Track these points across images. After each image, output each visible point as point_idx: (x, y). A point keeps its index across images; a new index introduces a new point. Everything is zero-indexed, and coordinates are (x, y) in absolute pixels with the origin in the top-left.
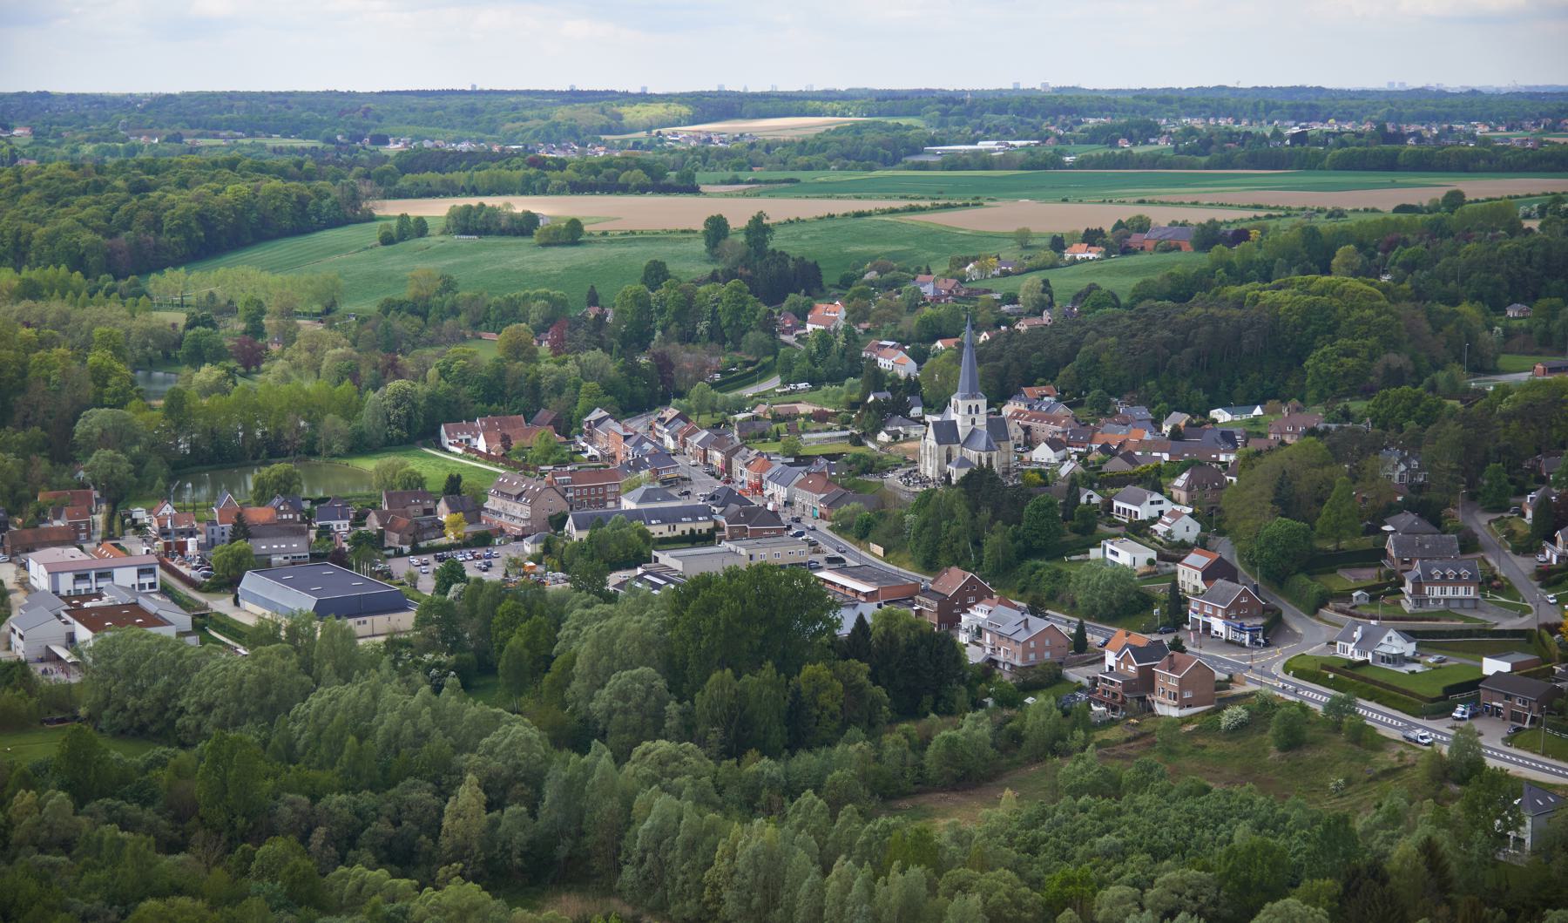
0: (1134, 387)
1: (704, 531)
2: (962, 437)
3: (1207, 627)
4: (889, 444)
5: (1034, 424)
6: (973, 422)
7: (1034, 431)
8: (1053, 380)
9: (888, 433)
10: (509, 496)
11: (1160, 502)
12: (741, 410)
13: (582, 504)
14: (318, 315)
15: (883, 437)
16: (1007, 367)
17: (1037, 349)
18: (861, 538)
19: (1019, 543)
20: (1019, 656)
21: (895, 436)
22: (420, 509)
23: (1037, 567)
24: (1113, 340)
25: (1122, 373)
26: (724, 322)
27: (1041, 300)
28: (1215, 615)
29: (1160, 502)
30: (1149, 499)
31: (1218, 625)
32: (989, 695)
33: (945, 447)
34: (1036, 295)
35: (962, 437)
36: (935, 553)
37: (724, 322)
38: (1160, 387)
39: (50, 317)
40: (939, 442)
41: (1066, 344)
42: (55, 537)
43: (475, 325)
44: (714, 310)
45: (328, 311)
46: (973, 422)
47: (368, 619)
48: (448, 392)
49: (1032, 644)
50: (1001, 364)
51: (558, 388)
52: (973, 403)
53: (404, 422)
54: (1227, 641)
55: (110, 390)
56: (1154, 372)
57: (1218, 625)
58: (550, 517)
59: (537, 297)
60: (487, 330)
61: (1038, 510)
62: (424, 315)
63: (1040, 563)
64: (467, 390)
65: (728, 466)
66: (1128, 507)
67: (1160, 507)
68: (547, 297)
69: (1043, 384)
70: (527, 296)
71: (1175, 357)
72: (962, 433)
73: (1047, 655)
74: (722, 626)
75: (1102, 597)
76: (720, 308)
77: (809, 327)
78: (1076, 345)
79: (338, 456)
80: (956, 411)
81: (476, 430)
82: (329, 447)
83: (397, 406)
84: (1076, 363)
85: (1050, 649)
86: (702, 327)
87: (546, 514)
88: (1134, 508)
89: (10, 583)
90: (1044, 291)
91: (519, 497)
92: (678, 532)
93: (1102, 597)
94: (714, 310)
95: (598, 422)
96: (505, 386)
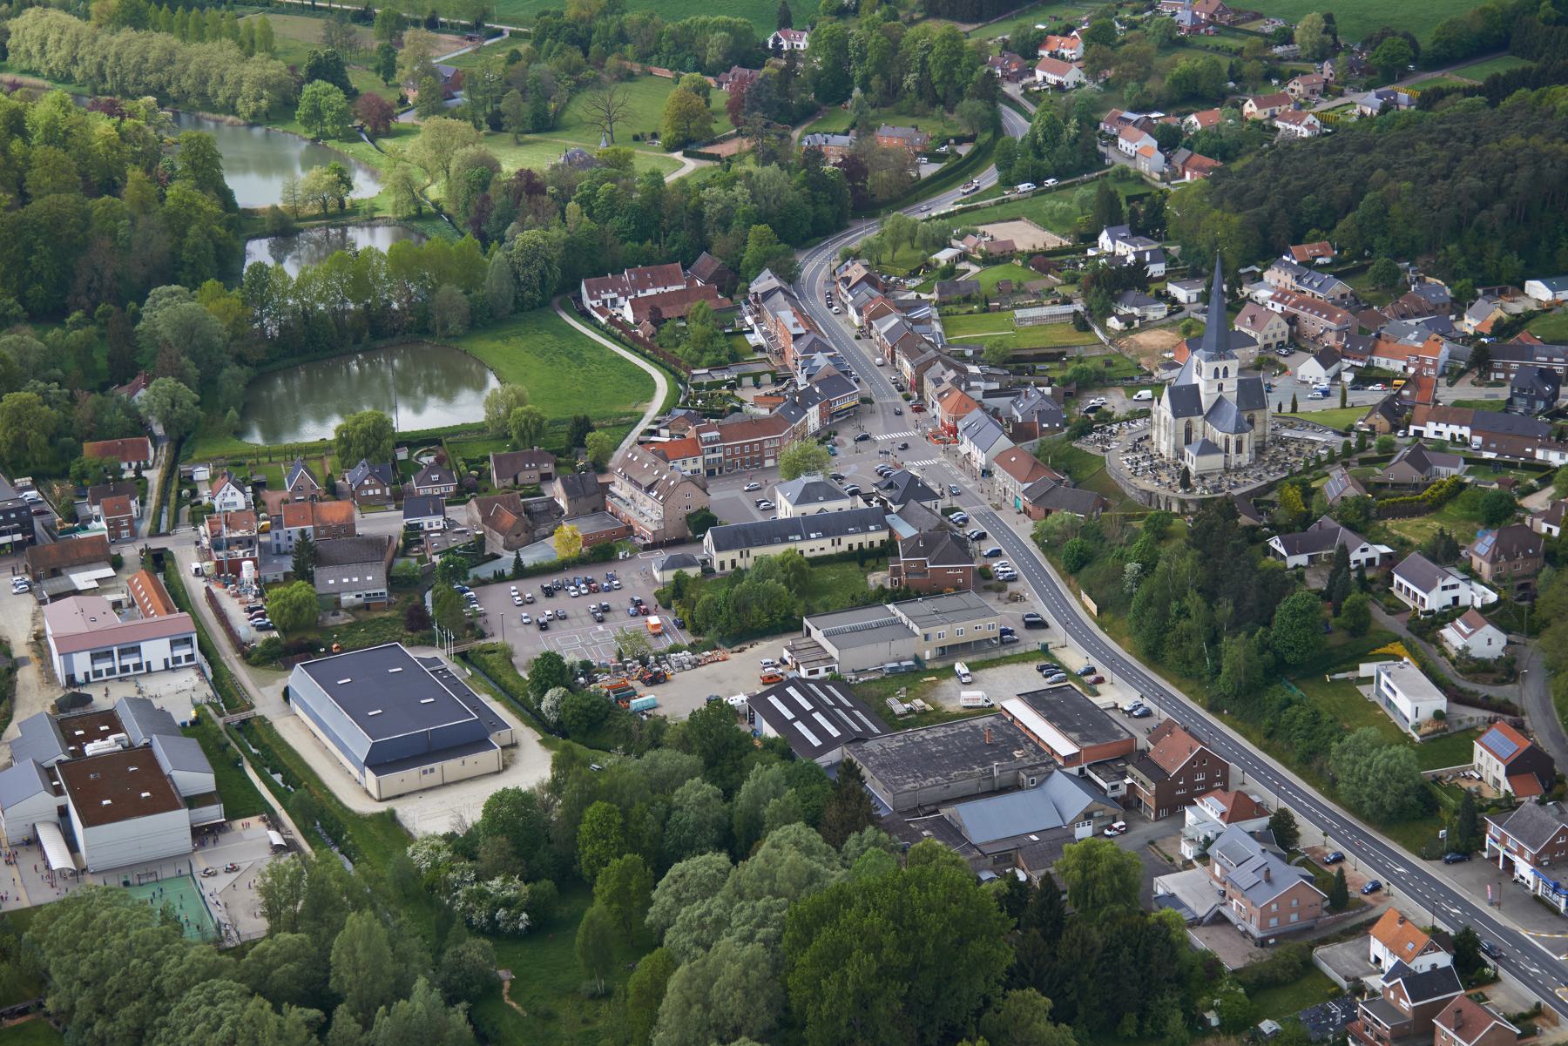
0: (1431, 248)
1: (877, 544)
2: (1206, 406)
3: (1510, 866)
4: (1122, 334)
5: (1303, 314)
6: (1220, 388)
7: (1301, 321)
8: (1329, 229)
9: (1120, 319)
10: (638, 485)
11: (1454, 587)
12: (945, 244)
13: (734, 464)
14: (466, 28)
15: (1113, 323)
16: (1272, 215)
17: (1312, 189)
18: (1071, 572)
19: (1268, 655)
20: (1256, 920)
21: (1128, 320)
22: (535, 475)
23: (1290, 703)
24: (1407, 185)
25: (1416, 232)
26: (935, 78)
27: (1322, 42)
28: (1521, 853)
29: (1454, 587)
30: (1440, 584)
31: (1524, 869)
32: (1211, 1007)
33: (1183, 421)
34: (1315, 38)
35: (1206, 406)
36: (1160, 643)
37: (935, 78)
38: (1464, 252)
39: (152, 56)
40: (1176, 415)
41: (1346, 187)
42: (86, 552)
43: (644, 58)
44: (924, 61)
45: (478, 26)
46: (1220, 388)
47: (436, 766)
48: (591, 234)
49: (1274, 907)
50: (1265, 209)
51: (725, 223)
52: (1221, 365)
53: (536, 282)
54: (1536, 898)
55: (190, 242)
56: (1457, 230)
57: (1524, 869)
58: (689, 516)
59: (717, 27)
60: (658, 65)
61: (1294, 616)
62: (583, 44)
63: (1297, 693)
64: (616, 223)
65: (918, 384)
66: (1413, 588)
67: (1454, 593)
68: (729, 27)
69: (1316, 238)
70: (705, 24)
71: (1485, 213)
72: (1206, 402)
73: (1294, 917)
74: (850, 989)
75: (1371, 797)
76: (930, 59)
77: (1039, 75)
78: (1360, 188)
79: (457, 337)
80: (1199, 373)
81: (623, 285)
82: (444, 326)
83: (527, 264)
84: (1358, 214)
85: (1299, 911)
86: (910, 80)
87: (682, 512)
88: (1420, 593)
89: (20, 645)
90: (1326, 31)
91: (649, 489)
92: (844, 548)
93: (1371, 797)
94: (924, 61)
95: (767, 295)
96: (662, 216)
